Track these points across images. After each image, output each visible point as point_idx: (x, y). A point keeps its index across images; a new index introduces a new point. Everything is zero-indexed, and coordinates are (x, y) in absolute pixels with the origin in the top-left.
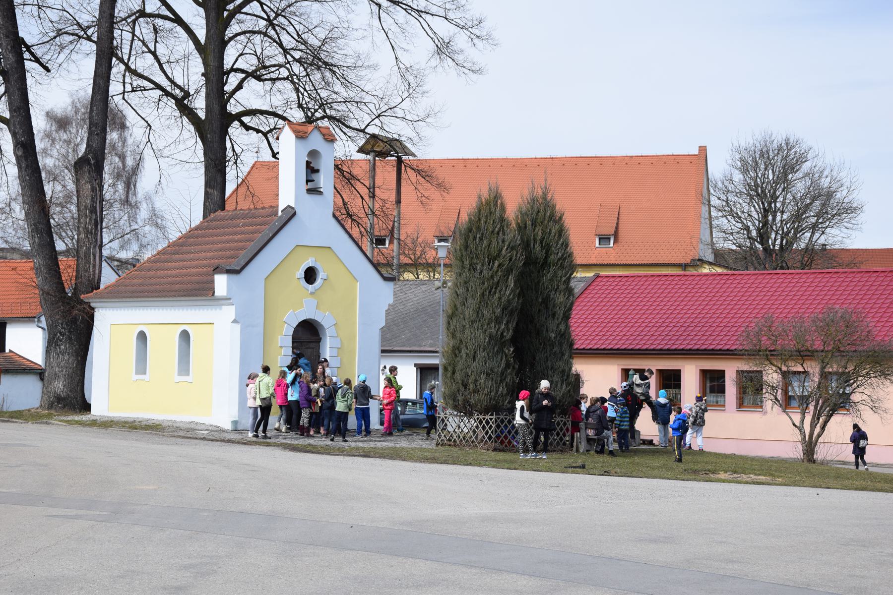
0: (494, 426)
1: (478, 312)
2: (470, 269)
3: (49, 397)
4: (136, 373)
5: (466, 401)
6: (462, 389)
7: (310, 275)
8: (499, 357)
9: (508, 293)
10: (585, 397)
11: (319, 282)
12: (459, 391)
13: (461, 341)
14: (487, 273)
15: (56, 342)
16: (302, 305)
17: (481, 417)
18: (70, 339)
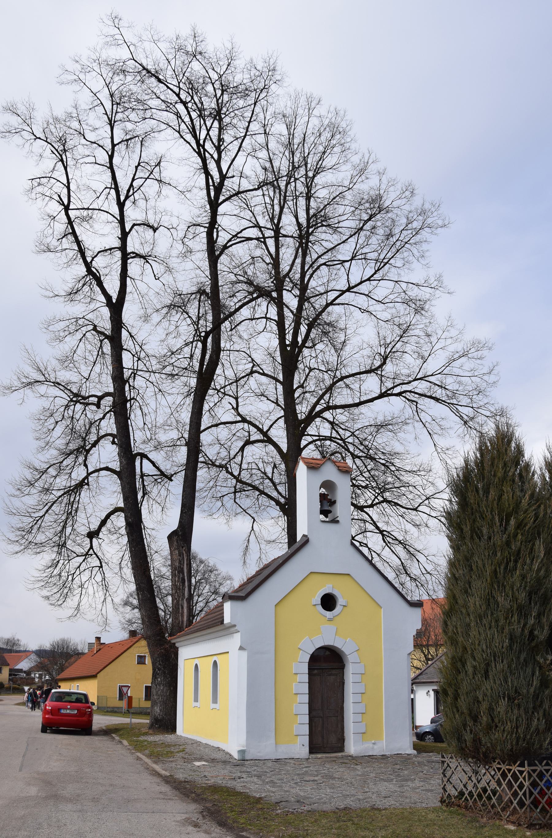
0: (526, 784)
1: (489, 600)
2: (472, 538)
5: (477, 741)
6: (470, 723)
7: (328, 602)
8: (529, 670)
9: (536, 567)
11: (338, 609)
12: (465, 725)
13: (465, 648)
14: (499, 539)
16: (326, 632)
17: (504, 767)
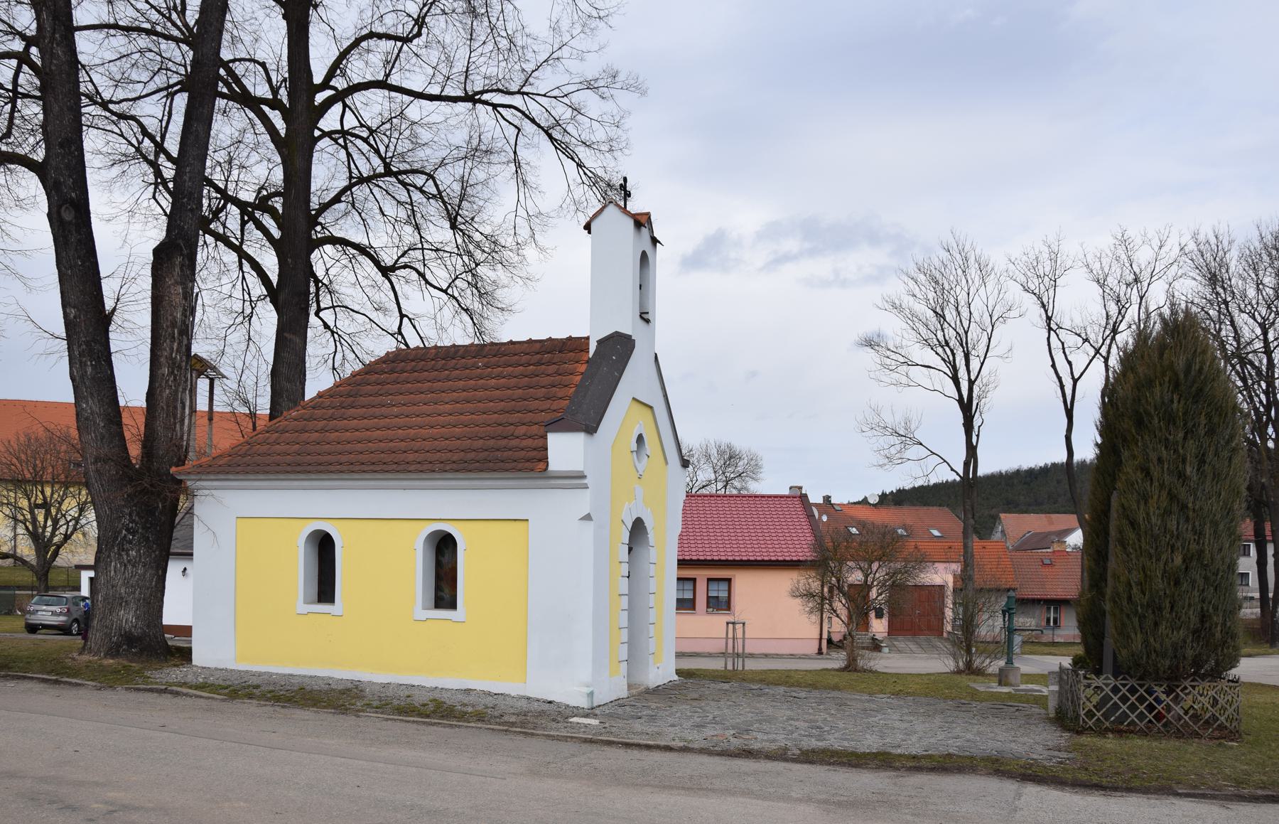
3: (108, 635)
4: (305, 602)
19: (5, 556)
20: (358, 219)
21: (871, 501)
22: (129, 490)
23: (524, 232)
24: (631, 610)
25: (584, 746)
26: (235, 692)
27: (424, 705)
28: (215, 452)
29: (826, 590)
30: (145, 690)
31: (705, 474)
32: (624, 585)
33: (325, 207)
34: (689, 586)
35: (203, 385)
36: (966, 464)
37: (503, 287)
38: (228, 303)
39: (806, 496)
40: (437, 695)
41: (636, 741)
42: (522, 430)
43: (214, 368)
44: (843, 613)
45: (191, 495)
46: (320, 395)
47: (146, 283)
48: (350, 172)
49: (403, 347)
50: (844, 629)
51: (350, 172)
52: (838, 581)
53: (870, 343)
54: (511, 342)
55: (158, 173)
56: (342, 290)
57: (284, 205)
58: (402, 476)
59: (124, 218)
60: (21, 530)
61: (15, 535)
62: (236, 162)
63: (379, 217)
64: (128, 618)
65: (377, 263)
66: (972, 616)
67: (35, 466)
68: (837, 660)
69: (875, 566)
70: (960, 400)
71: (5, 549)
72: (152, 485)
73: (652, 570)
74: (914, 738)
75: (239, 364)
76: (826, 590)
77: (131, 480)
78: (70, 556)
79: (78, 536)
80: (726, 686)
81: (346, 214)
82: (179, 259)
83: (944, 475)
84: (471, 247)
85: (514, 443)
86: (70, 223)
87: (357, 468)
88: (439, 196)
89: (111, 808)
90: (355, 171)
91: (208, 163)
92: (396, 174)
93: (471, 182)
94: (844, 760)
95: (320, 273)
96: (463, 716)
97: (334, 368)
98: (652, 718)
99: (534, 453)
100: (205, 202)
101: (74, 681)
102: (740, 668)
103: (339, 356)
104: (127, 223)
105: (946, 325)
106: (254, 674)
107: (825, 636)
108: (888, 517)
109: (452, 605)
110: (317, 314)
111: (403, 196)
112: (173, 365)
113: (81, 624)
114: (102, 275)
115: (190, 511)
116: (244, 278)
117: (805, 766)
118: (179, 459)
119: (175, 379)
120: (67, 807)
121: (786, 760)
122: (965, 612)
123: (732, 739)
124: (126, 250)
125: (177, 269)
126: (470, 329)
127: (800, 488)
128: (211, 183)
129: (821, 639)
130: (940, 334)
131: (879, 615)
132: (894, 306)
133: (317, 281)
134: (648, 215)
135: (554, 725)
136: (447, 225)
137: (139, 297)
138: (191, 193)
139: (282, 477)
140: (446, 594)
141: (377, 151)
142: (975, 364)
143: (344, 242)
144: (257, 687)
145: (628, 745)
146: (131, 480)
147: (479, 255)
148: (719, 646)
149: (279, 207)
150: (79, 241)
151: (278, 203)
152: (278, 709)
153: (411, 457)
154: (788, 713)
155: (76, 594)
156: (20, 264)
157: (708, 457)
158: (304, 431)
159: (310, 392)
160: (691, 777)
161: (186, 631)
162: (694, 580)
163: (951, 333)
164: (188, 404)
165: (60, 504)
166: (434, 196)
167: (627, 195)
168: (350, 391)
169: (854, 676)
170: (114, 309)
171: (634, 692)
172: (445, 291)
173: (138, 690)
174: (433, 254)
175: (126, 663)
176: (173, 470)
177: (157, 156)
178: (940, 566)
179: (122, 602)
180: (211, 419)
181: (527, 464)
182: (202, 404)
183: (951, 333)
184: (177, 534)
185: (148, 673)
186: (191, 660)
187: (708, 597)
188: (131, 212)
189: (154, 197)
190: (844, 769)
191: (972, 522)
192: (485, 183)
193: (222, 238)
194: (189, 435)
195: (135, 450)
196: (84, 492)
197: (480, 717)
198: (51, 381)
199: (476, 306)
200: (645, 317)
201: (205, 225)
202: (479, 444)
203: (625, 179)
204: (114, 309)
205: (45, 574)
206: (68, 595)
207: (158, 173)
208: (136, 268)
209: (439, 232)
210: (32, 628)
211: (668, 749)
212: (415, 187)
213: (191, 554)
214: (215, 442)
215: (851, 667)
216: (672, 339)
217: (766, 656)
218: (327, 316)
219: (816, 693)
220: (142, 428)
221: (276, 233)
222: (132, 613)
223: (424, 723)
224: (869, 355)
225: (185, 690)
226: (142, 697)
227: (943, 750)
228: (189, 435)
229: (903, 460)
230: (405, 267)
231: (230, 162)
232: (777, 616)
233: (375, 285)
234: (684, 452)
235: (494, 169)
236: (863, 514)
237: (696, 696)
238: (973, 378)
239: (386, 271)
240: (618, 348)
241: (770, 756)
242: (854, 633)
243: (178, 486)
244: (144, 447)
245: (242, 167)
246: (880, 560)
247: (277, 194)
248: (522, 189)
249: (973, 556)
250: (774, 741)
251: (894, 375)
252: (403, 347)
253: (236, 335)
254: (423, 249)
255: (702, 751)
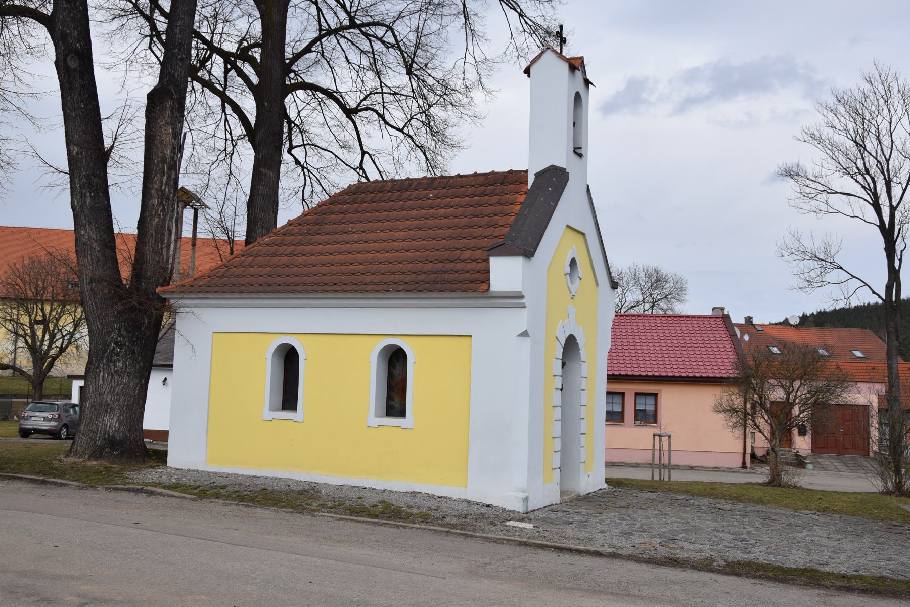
3: (93, 439)
4: (272, 409)
10: (359, 181)
15: (110, 356)
18: (133, 352)
19: (5, 367)
20: (327, 66)
21: (792, 322)
22: (119, 307)
23: (471, 76)
24: (564, 420)
25: (519, 549)
26: (204, 491)
27: (374, 506)
28: (196, 274)
29: (748, 406)
30: (123, 489)
31: (633, 296)
32: (557, 398)
33: (297, 56)
34: (618, 399)
35: (188, 214)
36: (889, 288)
37: (452, 126)
38: (211, 142)
39: (728, 316)
40: (386, 497)
41: (567, 545)
42: (467, 254)
43: (199, 201)
44: (766, 429)
45: (174, 312)
46: (290, 223)
47: (140, 123)
48: (320, 25)
49: (364, 180)
50: (767, 445)
51: (320, 25)
52: (760, 398)
53: (790, 173)
54: (459, 176)
55: (153, 27)
56: (312, 130)
57: (262, 55)
58: (360, 295)
59: (123, 67)
60: (21, 344)
61: (16, 348)
62: (221, 17)
63: (345, 64)
64: (112, 423)
65: (343, 107)
66: (900, 437)
67: (37, 286)
68: (761, 475)
69: (797, 384)
70: (882, 226)
71: (5, 361)
72: (139, 303)
73: (584, 384)
74: (843, 557)
75: (221, 196)
76: (748, 406)
77: (121, 298)
78: (64, 367)
79: (72, 349)
80: (653, 496)
81: (317, 62)
82: (170, 103)
83: (865, 298)
84: (425, 91)
85: (460, 266)
86: (75, 70)
87: (320, 288)
88: (397, 46)
89: (83, 601)
90: (324, 24)
91: (197, 18)
92: (359, 27)
93: (425, 32)
94: (771, 574)
95: (292, 114)
96: (408, 517)
97: (303, 200)
98: (583, 524)
99: (477, 276)
100: (193, 52)
101: (59, 481)
102: (666, 479)
103: (308, 189)
104: (125, 72)
105: (866, 154)
106: (222, 476)
107: (749, 450)
108: (809, 337)
109: (402, 414)
110: (289, 152)
111: (365, 45)
112: (162, 196)
113: (67, 430)
114: (102, 117)
115: (172, 327)
116: (226, 120)
117: (731, 578)
118: (164, 280)
119: (163, 209)
120: (43, 600)
121: (712, 571)
122: (891, 434)
123: (659, 548)
124: (124, 95)
125: (168, 112)
126: (424, 164)
127: (723, 309)
128: (199, 36)
129: (744, 453)
130: (860, 164)
131: (802, 432)
132: (813, 137)
133: (290, 122)
134: (582, 59)
135: (492, 528)
136: (404, 71)
137: (134, 136)
138: (181, 44)
139: (254, 296)
140: (396, 404)
141: (343, 6)
142: (897, 191)
143: (314, 88)
144: (224, 487)
145: (560, 549)
146: (121, 298)
147: (432, 98)
148: (646, 458)
149: (258, 57)
150: (83, 86)
151: (257, 53)
152: (241, 508)
153: (368, 278)
154: (713, 524)
155: (67, 401)
156: (31, 106)
157: (636, 280)
158: (275, 255)
159: (282, 220)
160: (620, 583)
161: (163, 436)
162: (623, 394)
163: (871, 162)
164: (174, 231)
165: (58, 320)
166: (393, 46)
167: (563, 41)
168: (317, 219)
169: (778, 491)
170: (112, 147)
171: (566, 498)
172: (401, 130)
173: (117, 489)
174: (392, 98)
175: (107, 464)
176: (159, 290)
177: (152, 11)
178: (864, 387)
179: (107, 408)
180: (194, 245)
181: (472, 285)
182: (187, 232)
183: (871, 162)
184: (159, 347)
185: (126, 474)
186: (166, 462)
187: (636, 411)
188: (130, 62)
189: (150, 48)
190: (771, 584)
191: (896, 343)
192: (438, 33)
193: (208, 84)
194: (174, 259)
195: (126, 272)
196: (79, 310)
197: (424, 518)
198: (56, 213)
199: (429, 143)
200: (578, 152)
201: (192, 72)
202: (429, 266)
203: (561, 27)
204: (112, 147)
205: (40, 384)
206: (60, 402)
207: (153, 27)
208: (132, 111)
209: (397, 79)
210: (25, 433)
211: (597, 554)
212: (377, 38)
213: (172, 366)
214: (196, 265)
215: (775, 481)
216: (609, 169)
217: (692, 468)
218: (299, 153)
219: (740, 506)
220: (133, 253)
221: (255, 80)
222: (115, 419)
223: (373, 523)
224: (790, 185)
225: (159, 490)
226: (118, 496)
227: (874, 571)
228: (174, 259)
229: (823, 284)
230: (367, 109)
231: (216, 16)
232: (701, 430)
233: (341, 126)
234: (614, 275)
235: (446, 20)
236: (785, 334)
237: (624, 504)
238: (895, 204)
239: (350, 113)
240: (554, 180)
241: (696, 566)
242: (777, 449)
243: (163, 305)
244: (134, 269)
245: (226, 21)
246: (801, 378)
247: (256, 45)
248: (470, 38)
249: (898, 377)
250: (700, 551)
251: (814, 203)
252: (364, 180)
253: (219, 170)
254: (382, 93)
255: (630, 558)
